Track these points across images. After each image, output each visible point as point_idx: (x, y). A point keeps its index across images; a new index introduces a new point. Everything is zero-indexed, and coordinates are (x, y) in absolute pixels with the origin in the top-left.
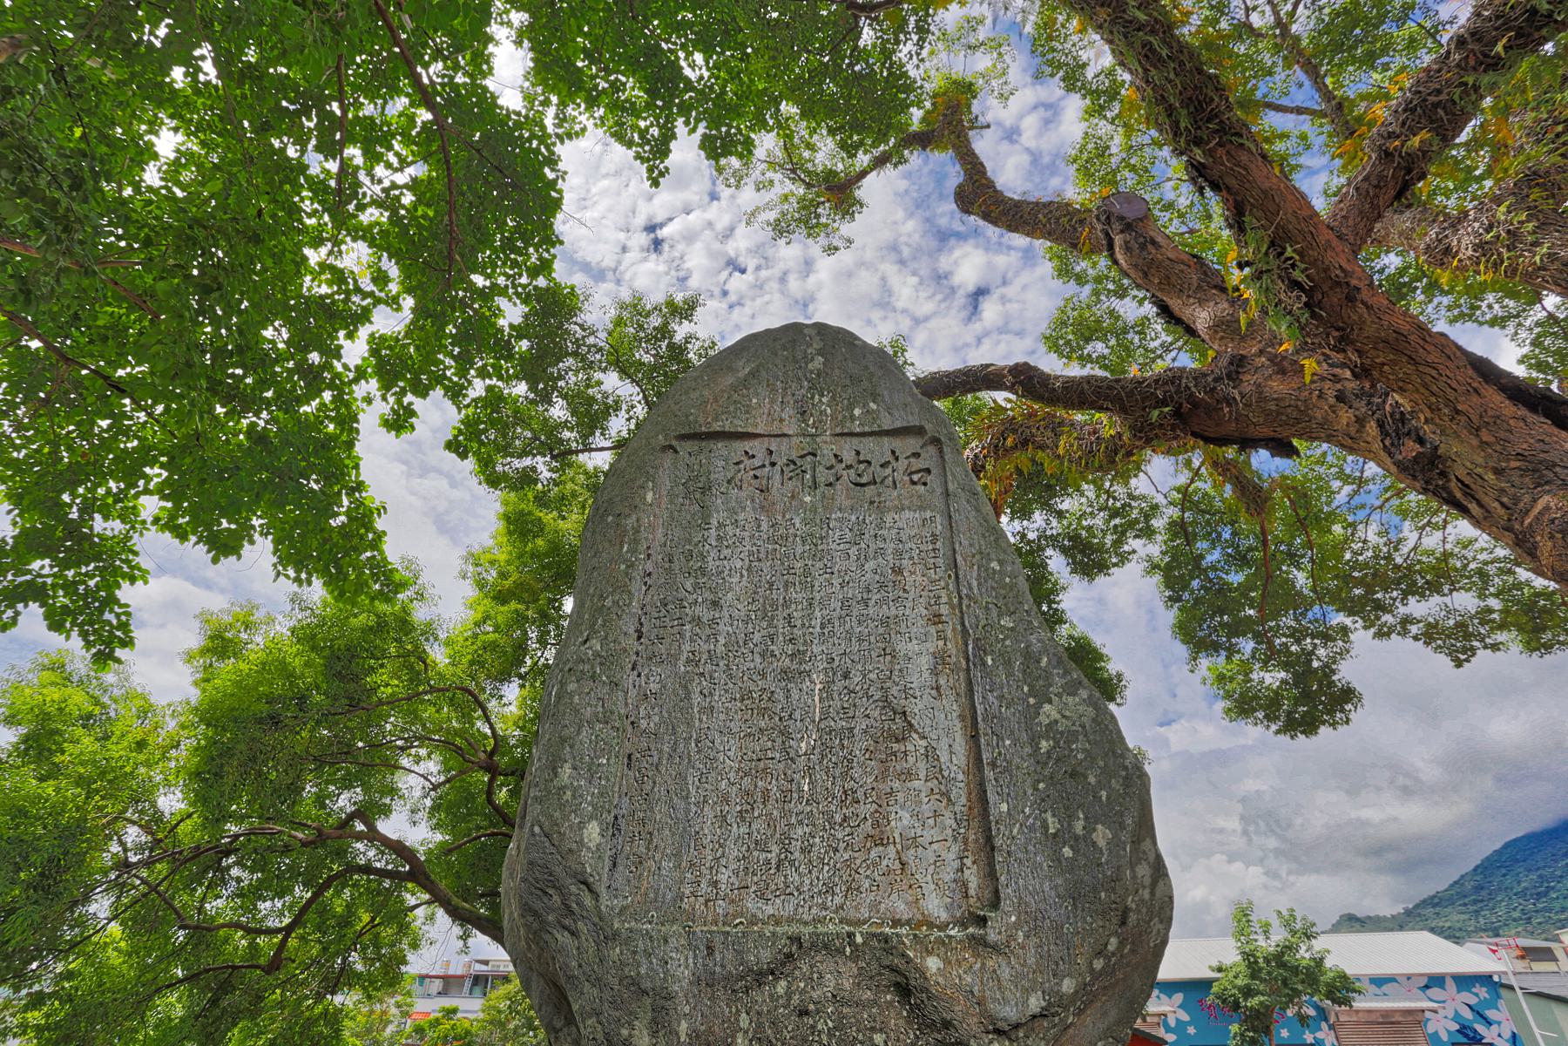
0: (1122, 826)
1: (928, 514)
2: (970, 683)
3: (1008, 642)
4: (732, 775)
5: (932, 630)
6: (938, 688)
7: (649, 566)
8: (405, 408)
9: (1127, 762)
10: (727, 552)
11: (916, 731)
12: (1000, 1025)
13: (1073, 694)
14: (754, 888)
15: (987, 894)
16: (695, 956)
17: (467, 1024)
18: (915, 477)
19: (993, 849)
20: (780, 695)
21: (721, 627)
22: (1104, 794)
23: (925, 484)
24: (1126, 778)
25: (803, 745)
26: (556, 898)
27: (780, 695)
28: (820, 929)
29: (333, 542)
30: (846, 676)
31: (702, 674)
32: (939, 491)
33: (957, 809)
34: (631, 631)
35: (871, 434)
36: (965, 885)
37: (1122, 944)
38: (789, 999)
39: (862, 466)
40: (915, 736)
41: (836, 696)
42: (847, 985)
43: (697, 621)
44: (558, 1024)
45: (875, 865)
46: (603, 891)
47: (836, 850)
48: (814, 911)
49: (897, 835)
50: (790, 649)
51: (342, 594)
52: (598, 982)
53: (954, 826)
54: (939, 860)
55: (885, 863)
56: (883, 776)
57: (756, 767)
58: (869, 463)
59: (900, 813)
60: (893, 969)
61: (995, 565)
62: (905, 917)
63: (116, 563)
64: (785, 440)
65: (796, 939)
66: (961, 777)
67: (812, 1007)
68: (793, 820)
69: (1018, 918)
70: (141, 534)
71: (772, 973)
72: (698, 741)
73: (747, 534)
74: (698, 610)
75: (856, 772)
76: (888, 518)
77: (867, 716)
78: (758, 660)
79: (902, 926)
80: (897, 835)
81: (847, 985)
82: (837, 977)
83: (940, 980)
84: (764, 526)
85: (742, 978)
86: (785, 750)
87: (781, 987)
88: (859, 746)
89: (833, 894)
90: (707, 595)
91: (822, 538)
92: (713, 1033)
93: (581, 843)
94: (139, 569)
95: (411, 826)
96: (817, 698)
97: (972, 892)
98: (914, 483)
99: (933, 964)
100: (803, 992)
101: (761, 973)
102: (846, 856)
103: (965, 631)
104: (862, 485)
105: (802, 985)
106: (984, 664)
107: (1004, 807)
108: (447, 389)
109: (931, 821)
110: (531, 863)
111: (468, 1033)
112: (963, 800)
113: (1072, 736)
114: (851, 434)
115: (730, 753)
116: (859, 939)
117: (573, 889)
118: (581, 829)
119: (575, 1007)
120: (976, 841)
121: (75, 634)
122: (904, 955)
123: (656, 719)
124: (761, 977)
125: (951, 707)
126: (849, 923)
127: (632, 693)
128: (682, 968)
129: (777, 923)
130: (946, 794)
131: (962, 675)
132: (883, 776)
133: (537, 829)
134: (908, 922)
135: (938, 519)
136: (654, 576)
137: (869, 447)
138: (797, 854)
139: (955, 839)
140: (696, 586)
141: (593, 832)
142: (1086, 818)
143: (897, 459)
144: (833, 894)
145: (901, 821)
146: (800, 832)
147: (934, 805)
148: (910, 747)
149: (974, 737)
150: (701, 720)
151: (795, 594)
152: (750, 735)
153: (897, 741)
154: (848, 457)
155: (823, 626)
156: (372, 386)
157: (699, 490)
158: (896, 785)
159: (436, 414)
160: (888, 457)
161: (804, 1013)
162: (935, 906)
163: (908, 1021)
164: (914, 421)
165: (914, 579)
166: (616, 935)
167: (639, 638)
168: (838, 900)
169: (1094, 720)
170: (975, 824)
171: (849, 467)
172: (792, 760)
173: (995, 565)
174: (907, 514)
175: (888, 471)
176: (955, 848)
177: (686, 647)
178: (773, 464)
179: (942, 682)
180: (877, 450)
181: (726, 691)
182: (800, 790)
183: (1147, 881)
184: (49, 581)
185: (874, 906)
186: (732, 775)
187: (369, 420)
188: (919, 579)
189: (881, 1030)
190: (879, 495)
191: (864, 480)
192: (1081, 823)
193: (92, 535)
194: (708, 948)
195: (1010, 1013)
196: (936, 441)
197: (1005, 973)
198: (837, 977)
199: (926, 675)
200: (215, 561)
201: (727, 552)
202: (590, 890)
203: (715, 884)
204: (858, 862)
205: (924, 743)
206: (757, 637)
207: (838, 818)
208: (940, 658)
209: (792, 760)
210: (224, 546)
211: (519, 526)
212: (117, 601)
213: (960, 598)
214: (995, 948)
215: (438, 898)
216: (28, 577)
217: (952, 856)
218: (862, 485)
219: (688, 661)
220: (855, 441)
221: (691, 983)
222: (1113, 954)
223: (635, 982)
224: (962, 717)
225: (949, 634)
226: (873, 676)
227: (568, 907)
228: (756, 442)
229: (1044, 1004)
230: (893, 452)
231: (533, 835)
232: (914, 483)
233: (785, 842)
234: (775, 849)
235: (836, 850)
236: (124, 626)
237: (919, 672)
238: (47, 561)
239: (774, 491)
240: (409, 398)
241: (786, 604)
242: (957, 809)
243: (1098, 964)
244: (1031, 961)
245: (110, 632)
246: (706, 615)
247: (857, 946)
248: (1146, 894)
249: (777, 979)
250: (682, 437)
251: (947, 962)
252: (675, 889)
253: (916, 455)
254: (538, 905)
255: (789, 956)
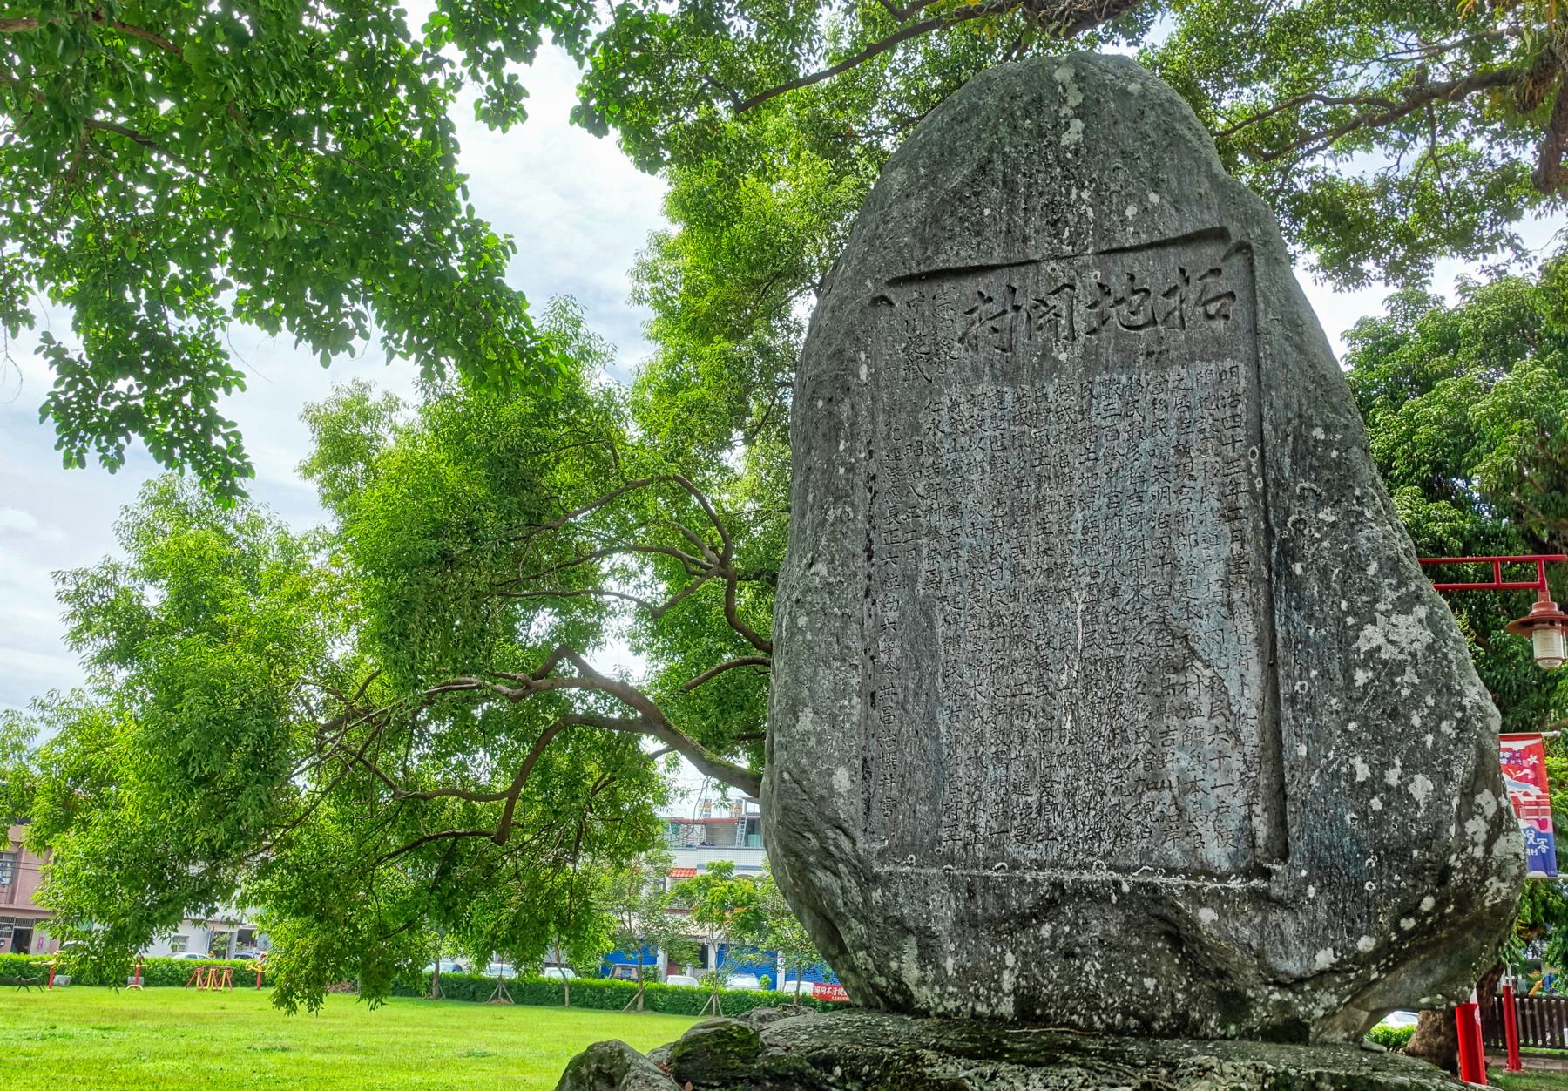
0: (1448, 777)
1: (1228, 363)
2: (1270, 600)
3: (1326, 544)
4: (985, 713)
5: (1226, 529)
6: (1230, 605)
7: (874, 468)
8: (506, 87)
9: (1465, 702)
10: (964, 440)
11: (1200, 659)
12: (1281, 978)
13: (1408, 612)
14: (1014, 832)
15: (1278, 845)
16: (957, 899)
17: (748, 886)
18: (1212, 309)
19: (1285, 797)
20: (1035, 621)
21: (963, 539)
22: (1429, 739)
23: (1226, 317)
24: (1460, 721)
25: (1064, 677)
26: (814, 841)
27: (1035, 621)
28: (1086, 876)
29: (458, 308)
30: (1114, 593)
31: (944, 598)
32: (1245, 326)
33: (1248, 749)
34: (859, 550)
35: (1151, 246)
36: (1252, 836)
37: (1440, 904)
38: (1055, 942)
39: (1136, 298)
40: (1198, 664)
41: (1102, 618)
42: (1114, 931)
43: (934, 532)
44: (835, 952)
45: (1147, 811)
46: (858, 834)
47: (1103, 794)
48: (1080, 856)
49: (1173, 779)
50: (1045, 562)
51: (483, 379)
52: (864, 919)
53: (1243, 768)
54: (1222, 808)
55: (1158, 808)
56: (1158, 713)
57: (1012, 706)
58: (1147, 292)
59: (1178, 754)
60: (1163, 919)
61: (1318, 433)
62: (1181, 865)
63: (202, 370)
64: (1031, 268)
65: (1057, 885)
66: (1253, 712)
67: (1078, 950)
68: (1055, 762)
69: (1310, 873)
70: (224, 328)
71: (1036, 917)
72: (945, 676)
73: (987, 413)
74: (935, 520)
75: (1125, 708)
76: (1172, 376)
77: (1140, 642)
78: (1007, 576)
79: (1177, 874)
80: (1173, 779)
81: (1114, 931)
82: (1102, 925)
83: (1215, 932)
84: (1008, 398)
85: (1005, 921)
86: (1043, 683)
87: (1046, 930)
88: (1129, 679)
89: (1101, 840)
90: (944, 499)
91: (1082, 412)
92: (980, 969)
93: (831, 789)
94: (232, 373)
95: (622, 657)
96: (1079, 622)
97: (1260, 842)
98: (1210, 317)
99: (1207, 915)
100: (1069, 935)
101: (1023, 916)
102: (1114, 801)
103: (1269, 532)
104: (1138, 328)
105: (1067, 929)
106: (1291, 573)
107: (1303, 750)
108: (557, 28)
109: (1215, 764)
110: (785, 808)
111: (751, 898)
112: (1255, 740)
113: (1399, 668)
114: (1123, 250)
115: (980, 688)
116: (1126, 888)
117: (830, 834)
118: (830, 775)
119: (847, 940)
120: (1269, 786)
121: (188, 467)
122: (1173, 906)
123: (897, 652)
124: (1024, 921)
125: (1246, 626)
126: (1118, 869)
127: (869, 623)
128: (943, 910)
129: (1041, 868)
130: (1234, 734)
131: (1262, 587)
132: (1158, 713)
133: (786, 776)
134: (1184, 871)
135: (1242, 366)
136: (879, 480)
137: (1149, 268)
138: (1060, 798)
139: (1243, 784)
140: (931, 489)
141: (842, 779)
142: (1404, 767)
143: (1187, 281)
144: (1101, 840)
145: (1178, 763)
146: (1063, 775)
147: (1219, 744)
148: (1192, 678)
149: (1271, 666)
150: (946, 652)
151: (1052, 491)
152: (1002, 667)
153: (1176, 671)
154: (1118, 286)
155: (1085, 531)
156: (452, 51)
157: (925, 355)
158: (1174, 722)
159: (553, 75)
160: (1174, 279)
161: (1070, 955)
162: (1216, 853)
163: (1181, 968)
164: (1211, 220)
165: (1203, 461)
166: (877, 877)
167: (870, 558)
168: (1106, 846)
169: (1429, 647)
170: (1268, 767)
171: (1118, 302)
172: (1051, 694)
173: (1318, 433)
174: (1200, 367)
175: (1174, 301)
176: (1243, 793)
177: (925, 565)
178: (1017, 308)
179: (1236, 596)
180: (1156, 271)
181: (973, 617)
182: (1061, 729)
183: (1481, 837)
184: (141, 402)
185: (1146, 854)
186: (985, 713)
187: (462, 110)
188: (1212, 458)
189: (1151, 975)
190: (1160, 341)
191: (1140, 319)
192: (1398, 771)
193: (170, 339)
194: (969, 891)
195: (1293, 966)
196: (1244, 248)
197: (1290, 928)
198: (1102, 925)
199: (1216, 588)
200: (325, 362)
201: (964, 440)
202: (846, 835)
203: (973, 828)
204: (1128, 807)
205: (1209, 673)
206: (1006, 549)
207: (1105, 759)
208: (1235, 566)
209: (1051, 694)
210: (328, 338)
211: (704, 213)
212: (221, 421)
213: (1266, 485)
214: (1280, 903)
215: (675, 741)
216: (118, 403)
217: (1237, 802)
218: (1138, 328)
219: (927, 582)
220: (1128, 258)
221: (954, 924)
222: (1428, 914)
223: (899, 921)
224: (1259, 641)
225: (1249, 533)
226: (1147, 592)
227: (828, 851)
228: (991, 278)
229: (1335, 960)
230: (1182, 271)
231: (784, 781)
232: (1210, 317)
233: (1046, 784)
234: (1036, 793)
235: (1103, 794)
236: (236, 450)
237: (1208, 585)
238: (131, 380)
239: (1020, 350)
240: (510, 67)
241: (1039, 507)
242: (1248, 749)
243: (1408, 924)
244: (1322, 915)
245: (225, 460)
246: (944, 524)
247: (1123, 895)
248: (1479, 853)
249: (1041, 923)
250: (895, 282)
251: (1222, 914)
252: (932, 833)
253: (1216, 272)
254: (799, 847)
255: (1052, 901)
